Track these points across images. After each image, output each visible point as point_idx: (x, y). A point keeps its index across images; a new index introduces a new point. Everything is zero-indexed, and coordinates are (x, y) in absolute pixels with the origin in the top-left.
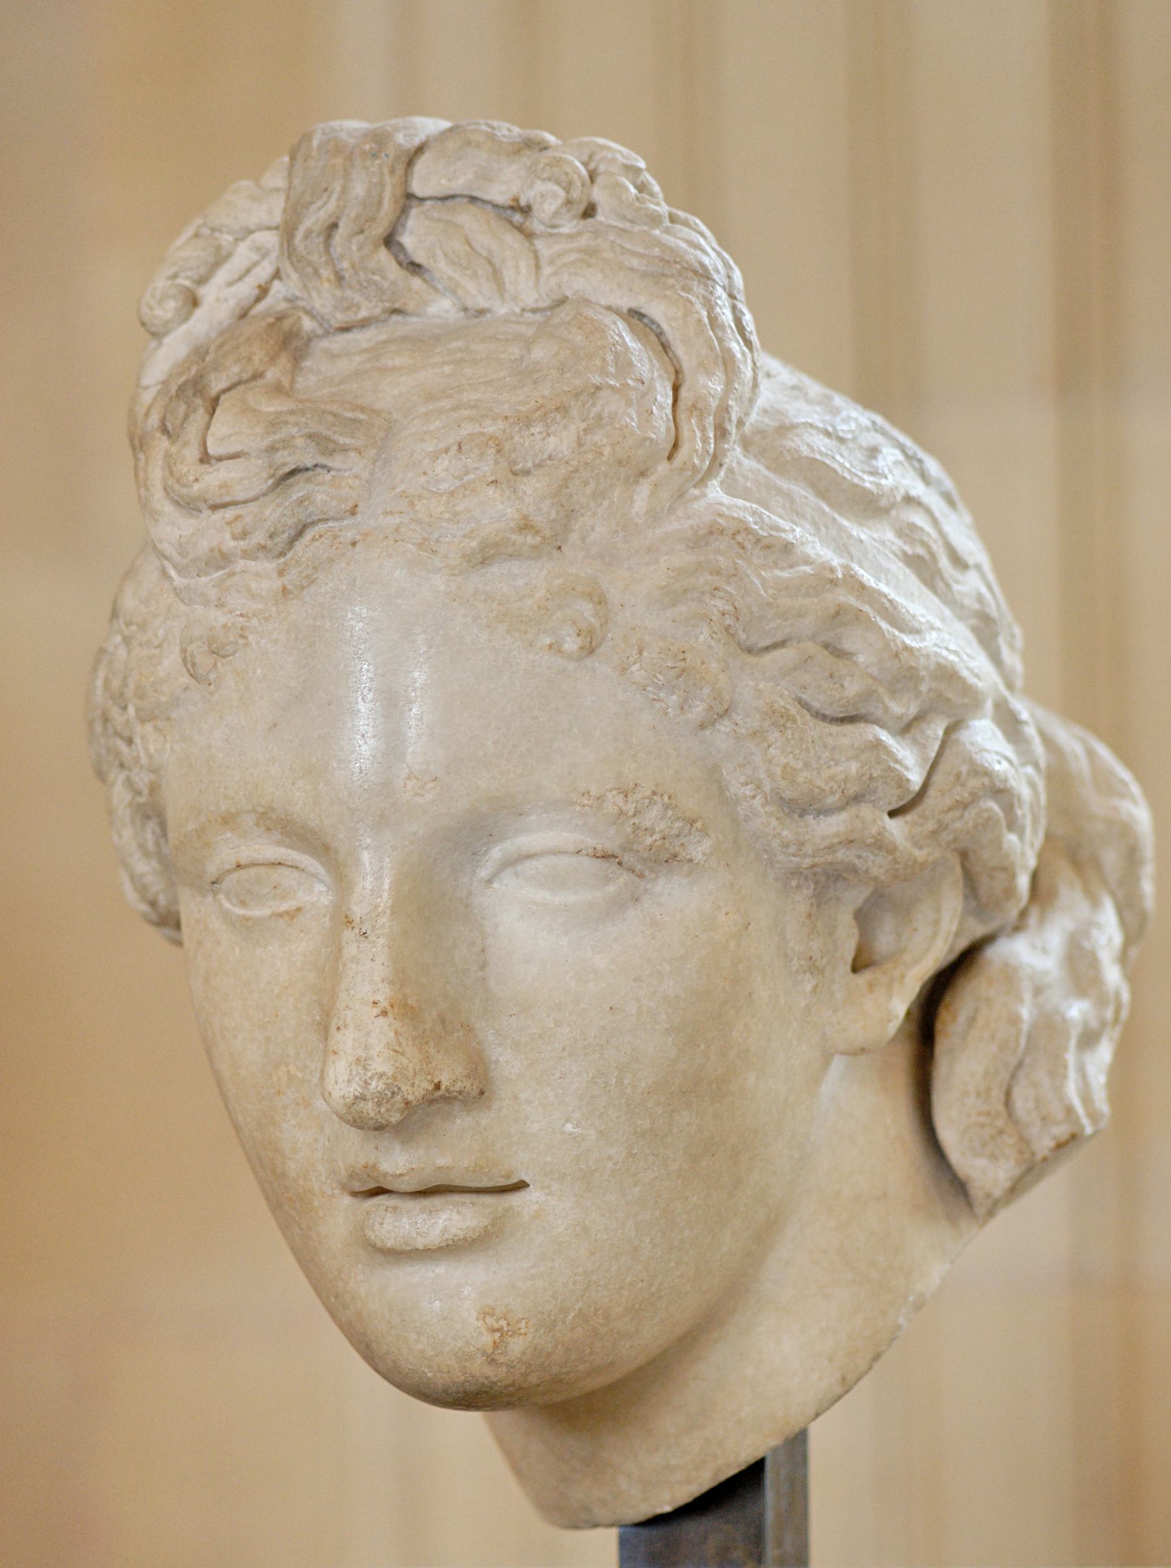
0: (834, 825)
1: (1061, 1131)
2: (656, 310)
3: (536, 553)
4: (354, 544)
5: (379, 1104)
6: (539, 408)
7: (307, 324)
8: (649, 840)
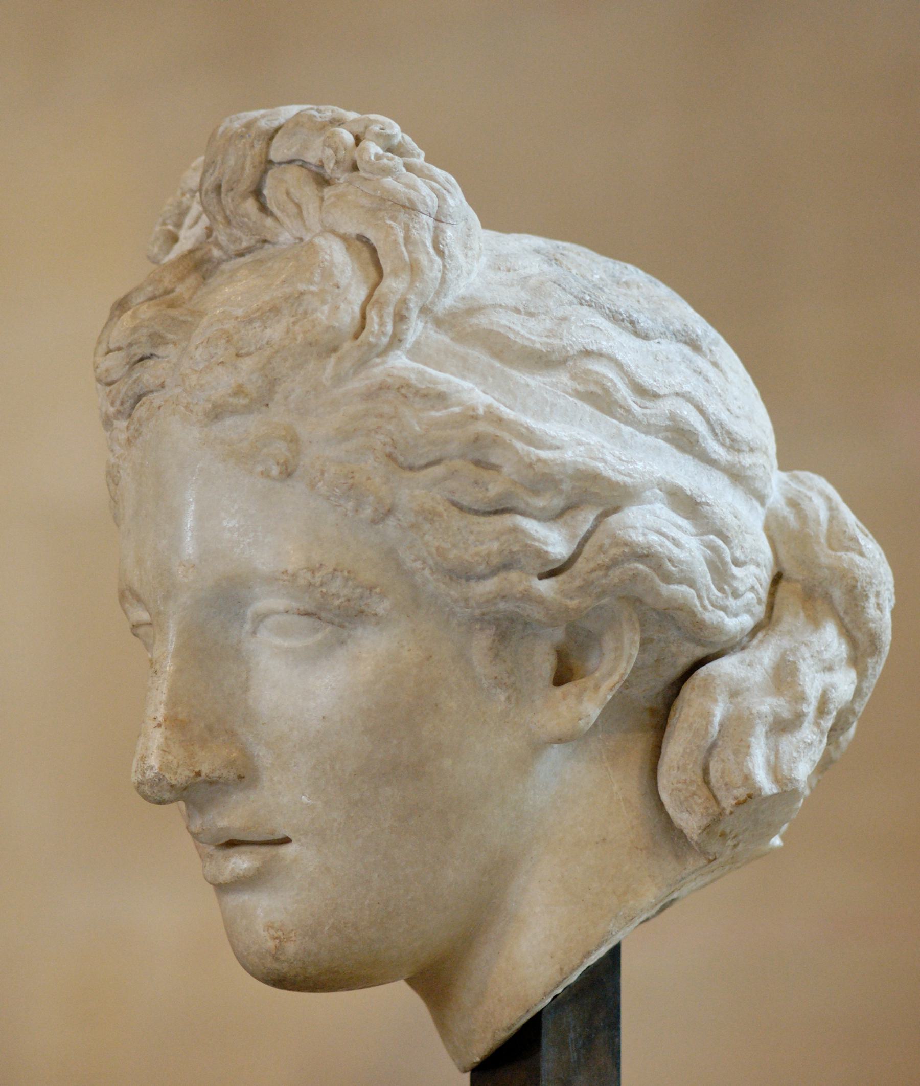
0: (489, 586)
1: (741, 793)
2: (371, 235)
3: (247, 410)
4: (159, 408)
5: (152, 787)
6: (258, 310)
7: (216, 253)
8: (337, 602)
